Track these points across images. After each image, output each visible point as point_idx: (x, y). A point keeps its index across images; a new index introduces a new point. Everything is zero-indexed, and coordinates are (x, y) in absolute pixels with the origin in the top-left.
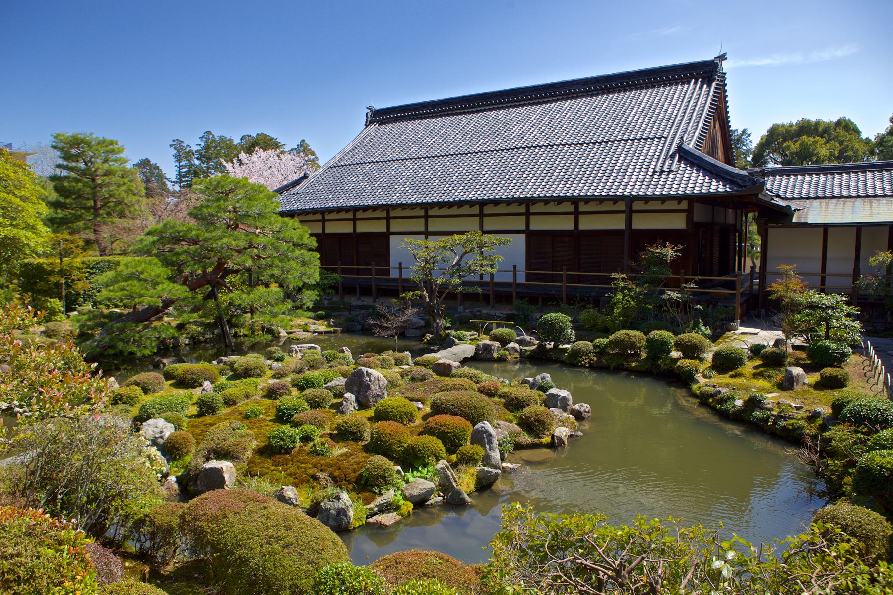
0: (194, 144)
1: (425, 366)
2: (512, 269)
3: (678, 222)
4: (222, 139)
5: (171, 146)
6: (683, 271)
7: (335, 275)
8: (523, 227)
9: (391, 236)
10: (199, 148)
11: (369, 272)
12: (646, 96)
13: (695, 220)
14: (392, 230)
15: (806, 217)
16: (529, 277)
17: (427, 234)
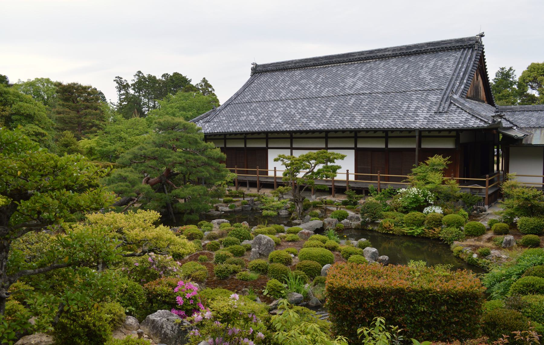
0: (131, 79)
1: (125, 204)
2: (346, 172)
3: (450, 145)
4: (150, 76)
5: (115, 81)
6: (452, 174)
7: (234, 174)
8: (353, 146)
9: (269, 150)
10: (134, 82)
11: (255, 173)
12: (433, 61)
13: (461, 142)
14: (269, 146)
15: (531, 140)
16: (356, 177)
17: (292, 149)
